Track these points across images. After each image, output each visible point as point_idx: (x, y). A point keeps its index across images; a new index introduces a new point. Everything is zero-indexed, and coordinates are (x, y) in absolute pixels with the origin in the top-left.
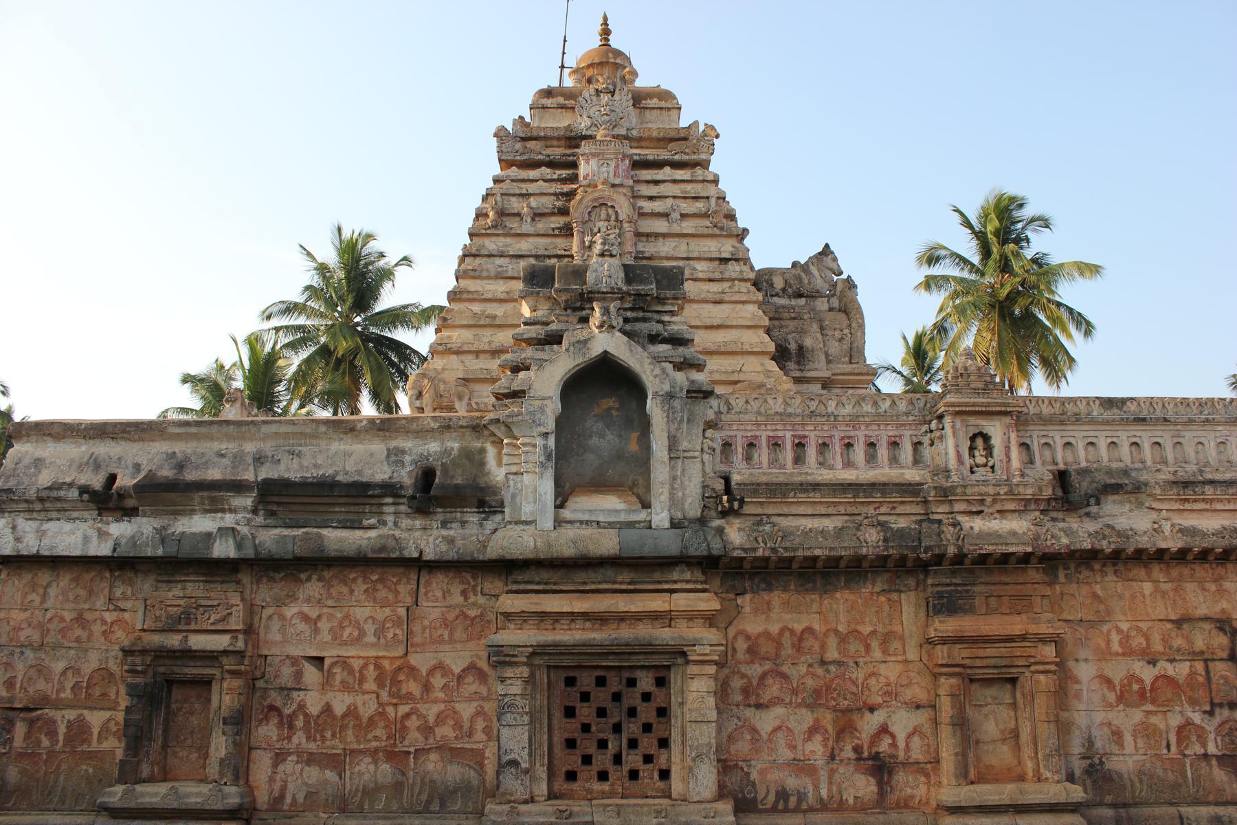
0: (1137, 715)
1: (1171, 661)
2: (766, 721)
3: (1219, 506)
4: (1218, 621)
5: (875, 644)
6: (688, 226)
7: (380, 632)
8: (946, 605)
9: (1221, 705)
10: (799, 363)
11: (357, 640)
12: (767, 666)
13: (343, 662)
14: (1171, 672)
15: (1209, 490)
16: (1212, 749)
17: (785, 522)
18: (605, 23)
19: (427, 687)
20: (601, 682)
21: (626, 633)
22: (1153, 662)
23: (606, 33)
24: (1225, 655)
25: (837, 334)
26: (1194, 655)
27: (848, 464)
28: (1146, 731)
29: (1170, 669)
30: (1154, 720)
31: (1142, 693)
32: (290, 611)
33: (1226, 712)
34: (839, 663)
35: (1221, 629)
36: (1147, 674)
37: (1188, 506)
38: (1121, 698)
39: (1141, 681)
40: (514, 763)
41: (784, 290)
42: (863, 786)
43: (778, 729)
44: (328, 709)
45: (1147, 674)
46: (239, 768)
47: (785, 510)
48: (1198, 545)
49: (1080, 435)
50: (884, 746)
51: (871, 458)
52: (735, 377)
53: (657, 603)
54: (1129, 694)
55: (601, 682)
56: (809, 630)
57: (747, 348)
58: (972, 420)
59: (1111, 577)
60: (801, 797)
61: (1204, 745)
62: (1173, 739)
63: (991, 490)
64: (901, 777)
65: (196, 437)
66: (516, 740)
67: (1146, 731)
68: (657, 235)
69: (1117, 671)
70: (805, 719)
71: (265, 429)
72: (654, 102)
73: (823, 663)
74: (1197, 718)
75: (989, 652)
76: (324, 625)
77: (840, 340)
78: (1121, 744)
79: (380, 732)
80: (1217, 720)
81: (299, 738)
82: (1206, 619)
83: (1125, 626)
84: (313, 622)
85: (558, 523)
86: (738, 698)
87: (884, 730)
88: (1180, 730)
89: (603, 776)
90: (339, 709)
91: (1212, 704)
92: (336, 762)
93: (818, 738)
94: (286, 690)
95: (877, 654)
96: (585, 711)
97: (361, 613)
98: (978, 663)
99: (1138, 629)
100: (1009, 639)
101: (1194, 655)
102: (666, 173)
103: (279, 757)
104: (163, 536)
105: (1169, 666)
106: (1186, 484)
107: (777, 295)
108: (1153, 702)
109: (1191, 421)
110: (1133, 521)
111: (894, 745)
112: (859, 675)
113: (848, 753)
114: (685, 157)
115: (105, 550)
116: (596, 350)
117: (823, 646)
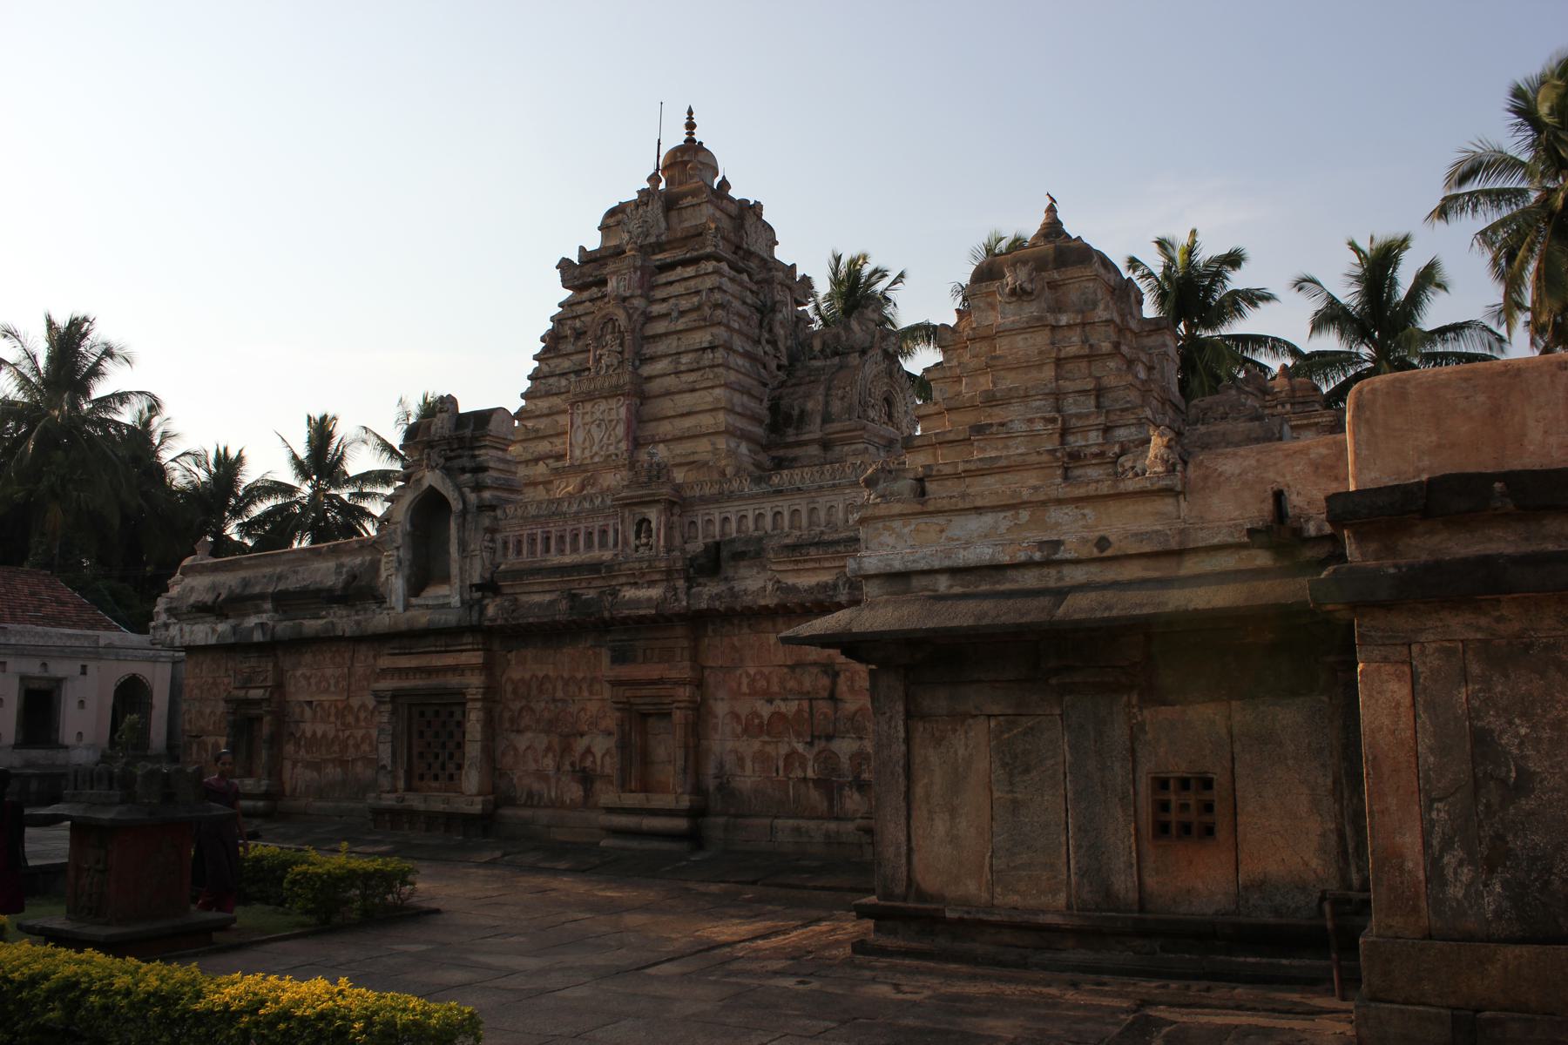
0: (756, 745)
1: (784, 700)
2: (522, 742)
3: (827, 564)
4: (824, 665)
5: (584, 687)
6: (681, 324)
7: (337, 683)
8: (619, 657)
9: (819, 738)
10: (797, 428)
11: (327, 690)
12: (524, 703)
13: (320, 704)
14: (783, 709)
15: (813, 551)
16: (810, 774)
17: (524, 598)
18: (690, 118)
19: (357, 719)
20: (437, 713)
21: (435, 681)
22: (770, 701)
23: (691, 126)
24: (826, 694)
25: (840, 393)
26: (801, 695)
27: (575, 550)
28: (762, 758)
29: (783, 707)
30: (769, 749)
31: (761, 725)
32: (299, 673)
33: (823, 743)
34: (563, 701)
35: (825, 672)
36: (765, 710)
37: (800, 566)
38: (745, 730)
39: (760, 717)
40: (384, 767)
41: (822, 351)
42: (575, 791)
43: (528, 748)
44: (314, 733)
45: (765, 710)
46: (275, 771)
47: (527, 589)
48: (792, 600)
49: (733, 509)
50: (588, 763)
51: (589, 545)
52: (691, 459)
53: (449, 660)
54: (752, 727)
55: (437, 713)
56: (546, 676)
57: (704, 430)
58: (637, 509)
59: (746, 630)
60: (541, 797)
61: (805, 771)
62: (781, 764)
63: (637, 565)
64: (598, 785)
65: (256, 566)
66: (385, 752)
67: (762, 758)
68: (661, 336)
69: (744, 708)
70: (542, 741)
71: (284, 558)
72: (688, 201)
73: (554, 700)
74: (800, 747)
75: (644, 692)
76: (313, 681)
77: (842, 398)
78: (743, 768)
79: (336, 748)
80: (816, 749)
81: (302, 752)
82: (815, 664)
83: (752, 671)
84: (308, 678)
85: (407, 607)
86: (507, 725)
87: (588, 751)
88: (787, 756)
89: (436, 778)
90: (319, 734)
91: (813, 736)
92: (317, 766)
93: (550, 755)
94: (297, 722)
95: (586, 694)
96: (1173, 798)
97: (329, 672)
98: (638, 701)
99: (762, 673)
100: (652, 682)
101: (801, 695)
102: (679, 272)
103: (294, 765)
104: (235, 629)
105: (782, 705)
106: (794, 548)
107: (814, 358)
108: (769, 734)
109: (821, 487)
110: (753, 583)
111: (594, 762)
112: (573, 709)
113: (567, 767)
114: (695, 254)
115: (212, 640)
116: (426, 484)
117: (554, 688)
